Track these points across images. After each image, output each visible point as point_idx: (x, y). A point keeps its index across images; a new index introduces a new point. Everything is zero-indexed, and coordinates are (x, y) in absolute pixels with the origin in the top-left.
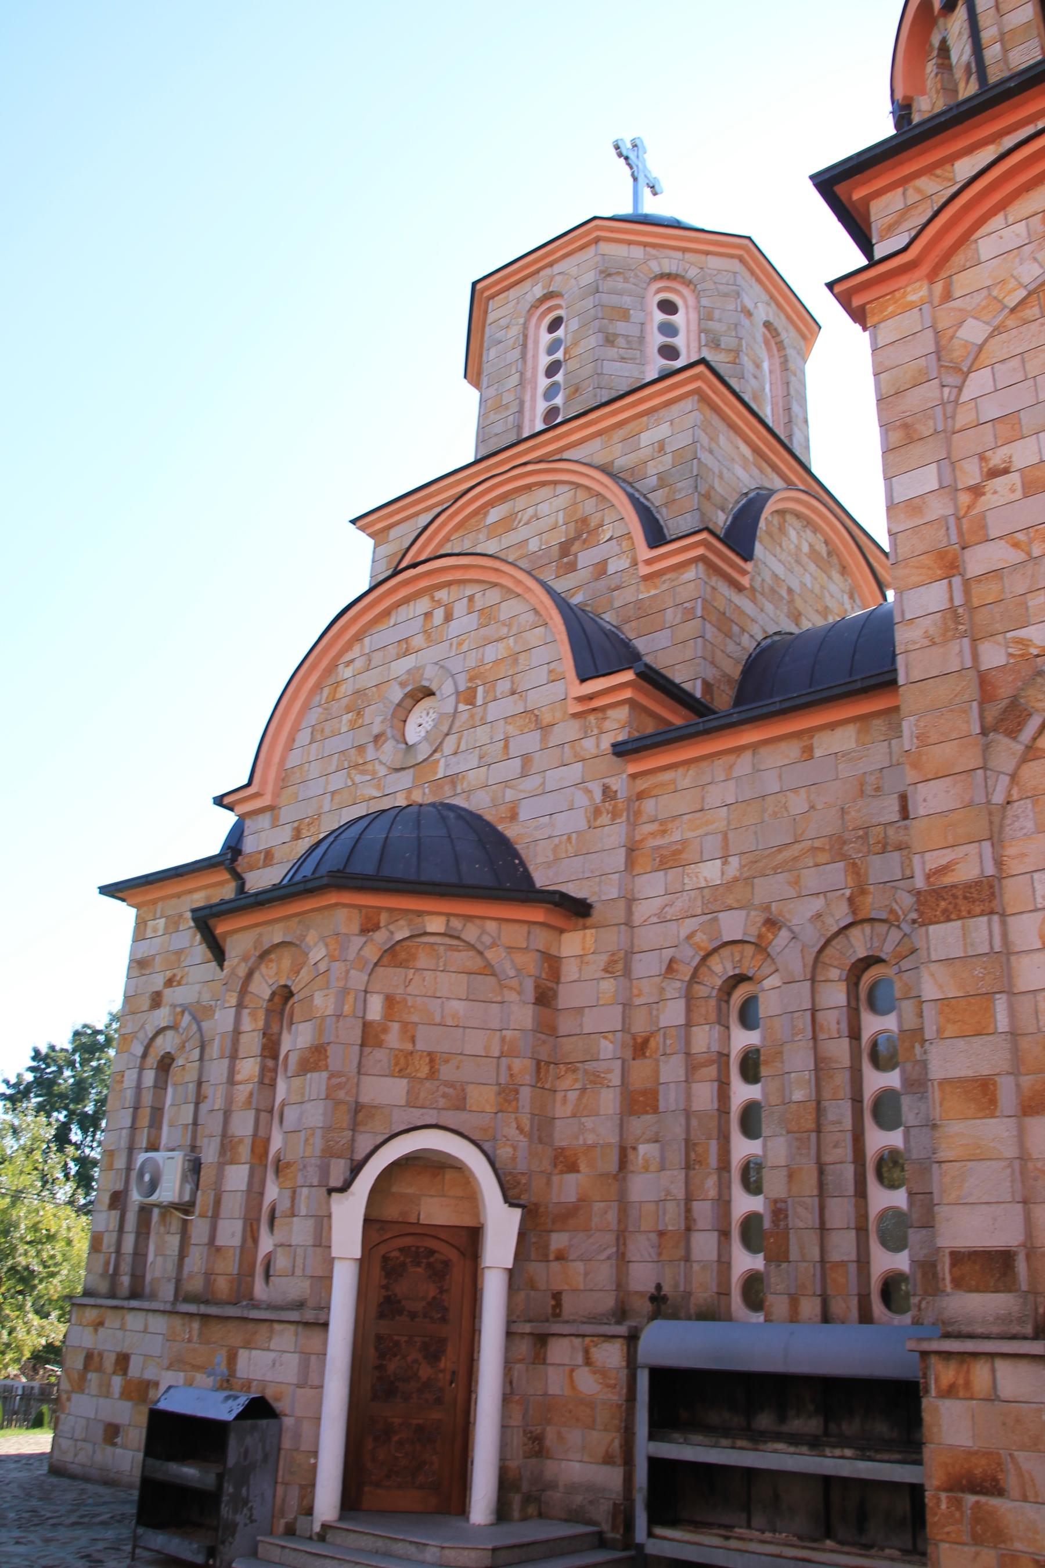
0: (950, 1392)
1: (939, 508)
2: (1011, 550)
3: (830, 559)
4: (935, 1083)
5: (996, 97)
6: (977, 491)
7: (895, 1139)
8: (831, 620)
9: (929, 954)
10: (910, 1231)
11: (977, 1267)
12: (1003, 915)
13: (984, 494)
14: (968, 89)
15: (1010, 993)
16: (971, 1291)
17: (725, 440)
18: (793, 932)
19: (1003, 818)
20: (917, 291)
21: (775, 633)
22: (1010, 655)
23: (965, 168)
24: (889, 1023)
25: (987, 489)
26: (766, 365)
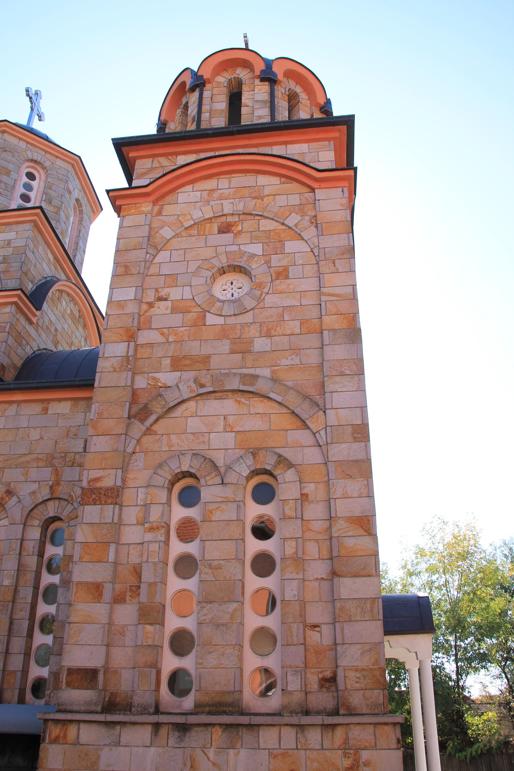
0: (55, 741)
1: (132, 308)
2: (160, 335)
3: (79, 319)
4: (74, 584)
5: (202, 135)
6: (151, 305)
7: (52, 609)
8: (73, 349)
9: (82, 519)
10: (52, 656)
11: (79, 677)
12: (121, 506)
13: (154, 307)
14: (192, 127)
15: (118, 543)
16: (74, 688)
17: (42, 248)
18: (19, 499)
19: (130, 460)
20: (146, 207)
21: (44, 349)
22: (149, 384)
23: (182, 160)
24: (59, 551)
25: (156, 305)
26: (72, 219)
